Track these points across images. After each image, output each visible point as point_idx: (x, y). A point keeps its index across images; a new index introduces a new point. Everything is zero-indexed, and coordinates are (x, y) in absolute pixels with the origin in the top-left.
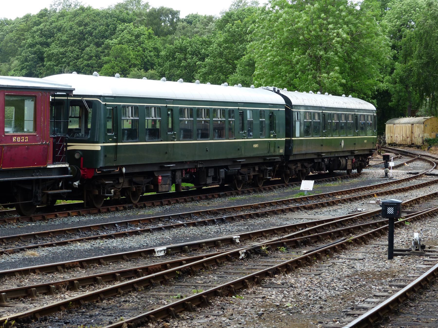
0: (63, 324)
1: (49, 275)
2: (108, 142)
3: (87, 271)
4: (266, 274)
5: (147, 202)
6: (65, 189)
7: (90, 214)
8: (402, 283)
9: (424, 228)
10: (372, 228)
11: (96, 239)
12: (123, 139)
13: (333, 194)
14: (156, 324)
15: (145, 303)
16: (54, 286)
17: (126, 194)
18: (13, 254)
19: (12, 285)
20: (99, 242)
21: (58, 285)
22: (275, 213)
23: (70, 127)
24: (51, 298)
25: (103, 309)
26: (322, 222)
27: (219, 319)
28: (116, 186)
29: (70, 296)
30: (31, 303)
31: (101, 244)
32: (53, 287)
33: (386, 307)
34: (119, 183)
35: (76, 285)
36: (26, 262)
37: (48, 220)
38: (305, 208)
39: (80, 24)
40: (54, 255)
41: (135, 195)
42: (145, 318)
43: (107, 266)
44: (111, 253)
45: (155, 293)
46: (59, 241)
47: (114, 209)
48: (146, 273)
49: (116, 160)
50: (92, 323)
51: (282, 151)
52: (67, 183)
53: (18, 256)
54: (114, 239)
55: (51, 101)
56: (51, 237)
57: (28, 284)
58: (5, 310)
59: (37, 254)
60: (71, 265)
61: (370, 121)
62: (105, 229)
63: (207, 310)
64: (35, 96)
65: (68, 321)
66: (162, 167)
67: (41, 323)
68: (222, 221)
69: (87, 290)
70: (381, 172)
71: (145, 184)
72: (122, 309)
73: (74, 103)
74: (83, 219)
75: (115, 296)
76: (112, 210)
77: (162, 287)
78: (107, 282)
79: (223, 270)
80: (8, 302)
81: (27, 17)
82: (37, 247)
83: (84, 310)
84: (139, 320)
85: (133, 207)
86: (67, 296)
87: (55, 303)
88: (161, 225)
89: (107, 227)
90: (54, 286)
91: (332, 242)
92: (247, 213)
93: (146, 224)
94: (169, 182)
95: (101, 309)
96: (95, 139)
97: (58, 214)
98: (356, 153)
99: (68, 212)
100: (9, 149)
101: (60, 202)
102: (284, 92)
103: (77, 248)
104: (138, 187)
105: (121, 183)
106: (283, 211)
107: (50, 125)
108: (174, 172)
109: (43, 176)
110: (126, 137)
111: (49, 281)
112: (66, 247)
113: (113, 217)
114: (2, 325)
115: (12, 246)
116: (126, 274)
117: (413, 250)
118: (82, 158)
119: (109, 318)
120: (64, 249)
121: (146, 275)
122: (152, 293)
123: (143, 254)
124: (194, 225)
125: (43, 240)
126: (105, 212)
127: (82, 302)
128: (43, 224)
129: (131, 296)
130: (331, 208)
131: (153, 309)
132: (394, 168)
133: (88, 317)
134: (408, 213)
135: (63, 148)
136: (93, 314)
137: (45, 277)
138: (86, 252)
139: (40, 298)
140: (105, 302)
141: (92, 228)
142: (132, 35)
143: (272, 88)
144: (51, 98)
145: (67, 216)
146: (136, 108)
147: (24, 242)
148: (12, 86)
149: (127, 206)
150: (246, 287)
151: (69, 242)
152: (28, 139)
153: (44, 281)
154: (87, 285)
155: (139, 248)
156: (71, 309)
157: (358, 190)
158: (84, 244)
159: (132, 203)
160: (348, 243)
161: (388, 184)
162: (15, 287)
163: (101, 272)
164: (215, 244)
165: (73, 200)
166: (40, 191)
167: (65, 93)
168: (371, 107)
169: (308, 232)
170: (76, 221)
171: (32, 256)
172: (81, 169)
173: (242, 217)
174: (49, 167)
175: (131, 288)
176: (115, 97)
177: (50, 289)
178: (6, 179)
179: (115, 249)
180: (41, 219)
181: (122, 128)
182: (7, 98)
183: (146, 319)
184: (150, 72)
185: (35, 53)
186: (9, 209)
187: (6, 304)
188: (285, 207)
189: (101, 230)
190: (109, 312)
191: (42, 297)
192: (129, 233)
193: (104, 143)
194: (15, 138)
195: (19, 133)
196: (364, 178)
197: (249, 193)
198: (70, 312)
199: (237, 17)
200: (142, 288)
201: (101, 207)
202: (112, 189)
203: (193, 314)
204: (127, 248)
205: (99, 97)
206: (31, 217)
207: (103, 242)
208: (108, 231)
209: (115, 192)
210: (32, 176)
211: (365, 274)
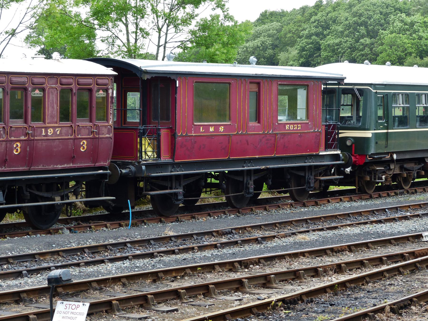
0: (328, 306)
1: (318, 258)
2: (379, 129)
3: (355, 255)
5: (418, 188)
6: (337, 175)
11: (366, 223)
12: (394, 126)
14: (419, 307)
15: (410, 286)
16: (321, 269)
17: (397, 180)
18: (285, 238)
19: (282, 268)
20: (369, 226)
21: (326, 268)
23: (341, 115)
24: (318, 281)
25: (368, 292)
28: (387, 172)
29: (337, 279)
30: (299, 286)
31: (371, 228)
32: (320, 270)
34: (390, 169)
35: (343, 268)
36: (297, 246)
37: (321, 205)
39: (355, 15)
40: (324, 240)
41: (406, 181)
42: (408, 301)
43: (375, 250)
44: (379, 237)
45: (420, 277)
46: (330, 226)
47: (386, 195)
48: (413, 257)
49: (387, 147)
50: (356, 306)
52: (339, 169)
53: (289, 240)
54: (384, 224)
55: (322, 89)
56: (323, 222)
57: (297, 267)
58: (273, 292)
59: (308, 239)
60: (339, 249)
62: (375, 214)
64: (308, 85)
65: (334, 303)
67: (307, 304)
69: (354, 273)
71: (415, 170)
72: (386, 292)
73: (346, 92)
74: (355, 204)
75: (381, 279)
76: (383, 196)
78: (374, 266)
80: (277, 284)
81: (304, 9)
82: (308, 231)
83: (349, 293)
84: (402, 303)
85: (405, 193)
86: (334, 279)
87: (322, 285)
89: (377, 212)
90: (321, 269)
93: (416, 210)
95: (366, 292)
96: (367, 126)
97: (330, 200)
99: (340, 197)
100: (282, 136)
101: (333, 188)
103: (346, 233)
104: (409, 173)
105: (392, 169)
107: (321, 113)
109: (316, 162)
110: (396, 124)
111: (318, 264)
112: (336, 232)
113: (384, 203)
114: (269, 306)
115: (284, 231)
116: (392, 258)
118: (354, 145)
119: (374, 300)
120: (334, 233)
121: (412, 259)
122: (417, 277)
123: (410, 239)
125: (315, 224)
126: (377, 198)
127: (348, 285)
128: (316, 210)
129: (396, 279)
131: (417, 293)
133: (353, 299)
135: (335, 136)
136: (359, 296)
137: (314, 261)
138: (355, 236)
139: (308, 280)
140: (371, 285)
141: (362, 213)
142: (405, 24)
144: (323, 86)
145: (339, 201)
146: (407, 95)
147: (296, 226)
148: (284, 76)
149: (398, 191)
151: (339, 227)
152: (301, 127)
153: (313, 264)
154: (354, 268)
155: (408, 233)
156: (336, 291)
158: (354, 229)
159: (404, 189)
162: (285, 270)
163: (368, 256)
165: (345, 186)
166: (312, 177)
167: (337, 82)
170: (348, 206)
171: (303, 240)
172: (352, 155)
174: (321, 153)
176: (385, 85)
177: (318, 272)
178: (280, 166)
179: (384, 234)
180: (314, 204)
181: (393, 115)
182: (280, 88)
183: (409, 302)
185: (312, 43)
187: (275, 285)
189: (372, 215)
190: (374, 295)
191: (310, 280)
192: (399, 218)
193: (375, 130)
194: (288, 126)
195: (292, 121)
198: (336, 294)
200: (408, 272)
201: (373, 192)
202: (383, 175)
204: (396, 233)
206: (304, 203)
207: (373, 227)
208: (379, 216)
209: (386, 179)
210: (305, 163)
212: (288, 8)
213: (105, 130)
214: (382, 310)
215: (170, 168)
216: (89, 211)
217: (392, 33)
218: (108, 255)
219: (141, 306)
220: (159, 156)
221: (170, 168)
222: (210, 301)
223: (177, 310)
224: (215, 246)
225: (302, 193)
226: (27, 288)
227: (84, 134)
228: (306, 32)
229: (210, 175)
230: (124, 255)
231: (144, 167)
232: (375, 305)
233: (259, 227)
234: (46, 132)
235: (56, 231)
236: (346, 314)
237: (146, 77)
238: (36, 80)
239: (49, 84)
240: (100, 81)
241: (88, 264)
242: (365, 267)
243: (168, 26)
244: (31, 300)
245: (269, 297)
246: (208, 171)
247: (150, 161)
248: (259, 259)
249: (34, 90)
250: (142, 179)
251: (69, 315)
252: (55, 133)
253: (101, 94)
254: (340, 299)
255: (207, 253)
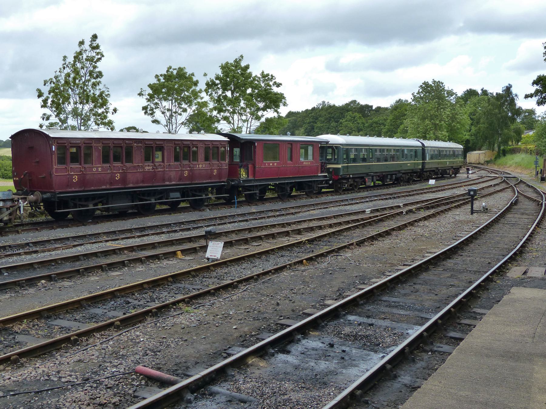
4: (416, 221)
7: (337, 195)
8: (478, 226)
9: (487, 201)
10: (462, 201)
11: (340, 206)
13: (444, 186)
22: (418, 194)
26: (440, 198)
27: (395, 241)
33: (472, 236)
38: (431, 192)
39: (329, 113)
51: (420, 167)
52: (327, 182)
61: (460, 153)
63: (390, 237)
66: (367, 174)
68: (394, 198)
70: (466, 175)
73: (329, 147)
74: (334, 197)
77: (370, 226)
79: (396, 219)
81: (307, 110)
87: (324, 233)
88: (367, 200)
91: (444, 207)
92: (405, 194)
94: (371, 181)
98: (454, 167)
101: (323, 190)
102: (421, 141)
106: (421, 193)
108: (373, 176)
112: (327, 209)
117: (482, 210)
124: (382, 199)
127: (336, 233)
130: (443, 192)
132: (471, 174)
134: (479, 194)
143: (416, 139)
149: (352, 191)
150: (407, 227)
157: (455, 184)
160: (452, 207)
161: (469, 181)
162: (306, 227)
164: (392, 208)
166: (315, 185)
169: (433, 203)
173: (403, 196)
175: (356, 227)
179: (348, 210)
182: (301, 146)
184: (361, 133)
185: (310, 126)
186: (302, 193)
187: (303, 234)
188: (422, 192)
190: (347, 238)
195: (306, 161)
196: (457, 178)
197: (406, 185)
198: (331, 237)
203: (384, 239)
205: (340, 144)
211: (460, 221)
212: (300, 110)
213: (224, 165)
214: (352, 244)
215: (253, 182)
216: (217, 201)
217: (346, 121)
218: (227, 221)
219: (245, 243)
220: (248, 177)
221: (253, 182)
222: (275, 241)
223: (261, 245)
224: (274, 216)
225: (311, 192)
226: (193, 235)
227: (215, 167)
228: (308, 121)
229: (270, 185)
230: (234, 220)
231: (241, 181)
232: (348, 242)
233: (293, 208)
234: (199, 166)
235: (204, 210)
236: (336, 246)
237: (242, 141)
238: (194, 143)
239: (200, 145)
240: (222, 143)
241: (219, 224)
242: (342, 225)
243: (252, 118)
244: (196, 241)
245: (301, 239)
246: (269, 183)
247: (244, 179)
248: (295, 222)
249: (193, 147)
250: (241, 187)
251: (215, 248)
252: (202, 167)
253: (223, 149)
254: (332, 239)
255: (271, 219)
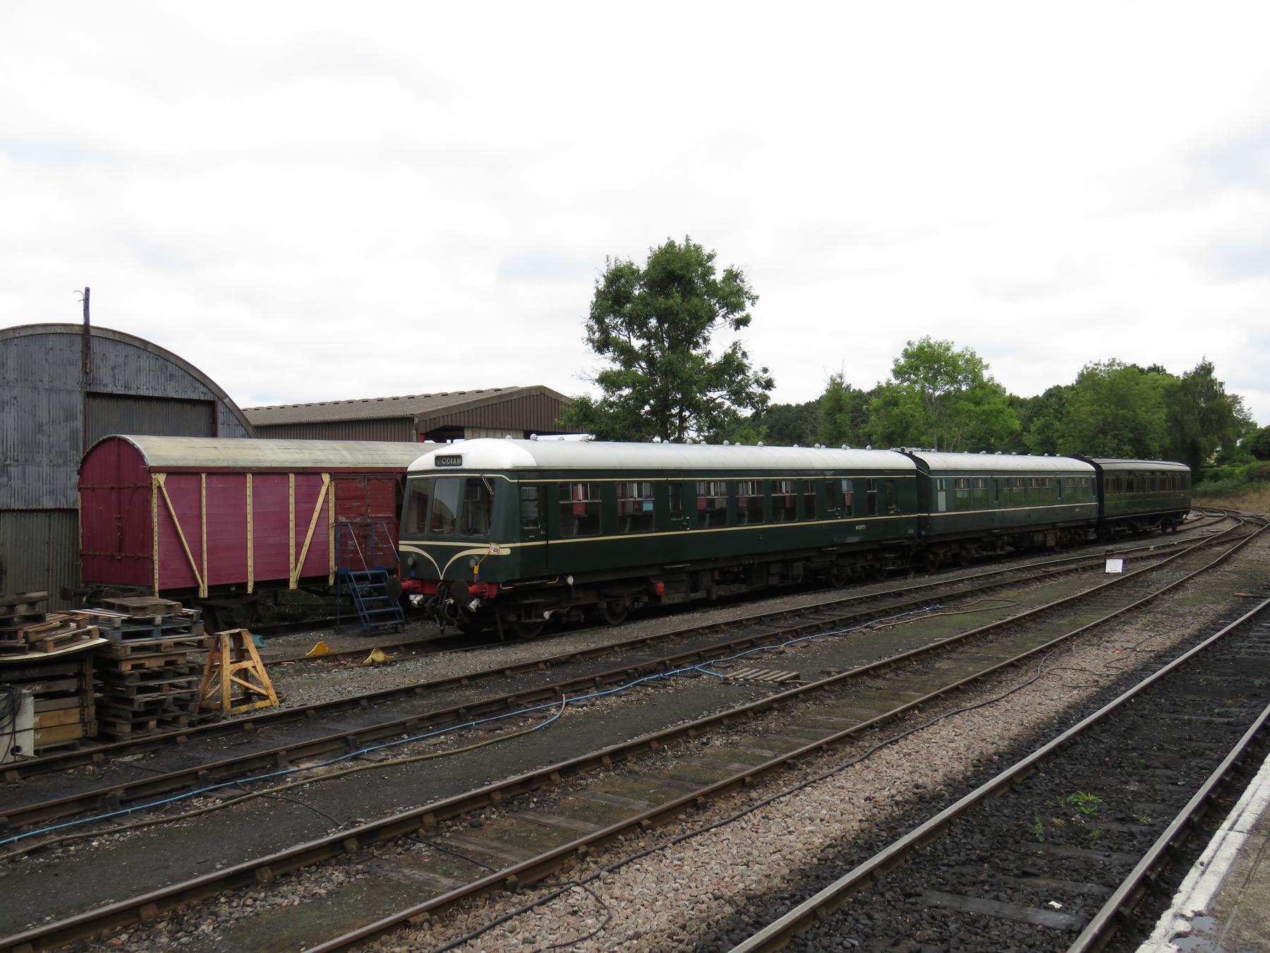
168: (1187, 468)
199: (697, 342)
